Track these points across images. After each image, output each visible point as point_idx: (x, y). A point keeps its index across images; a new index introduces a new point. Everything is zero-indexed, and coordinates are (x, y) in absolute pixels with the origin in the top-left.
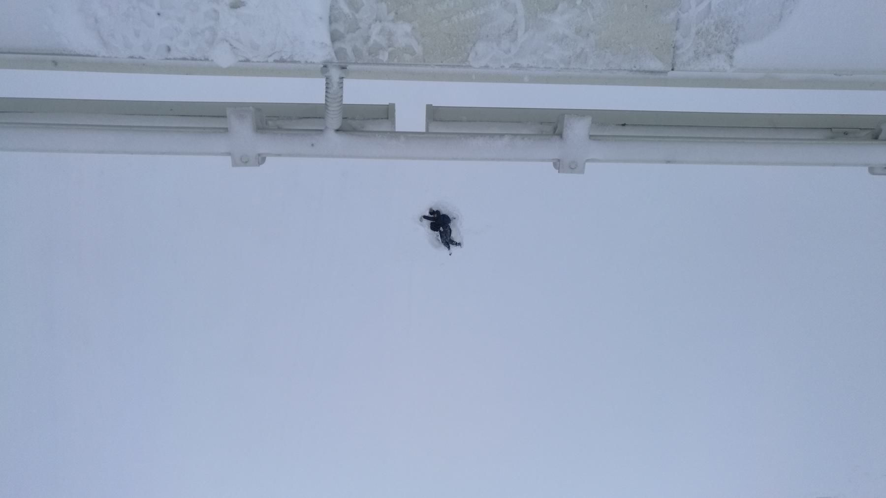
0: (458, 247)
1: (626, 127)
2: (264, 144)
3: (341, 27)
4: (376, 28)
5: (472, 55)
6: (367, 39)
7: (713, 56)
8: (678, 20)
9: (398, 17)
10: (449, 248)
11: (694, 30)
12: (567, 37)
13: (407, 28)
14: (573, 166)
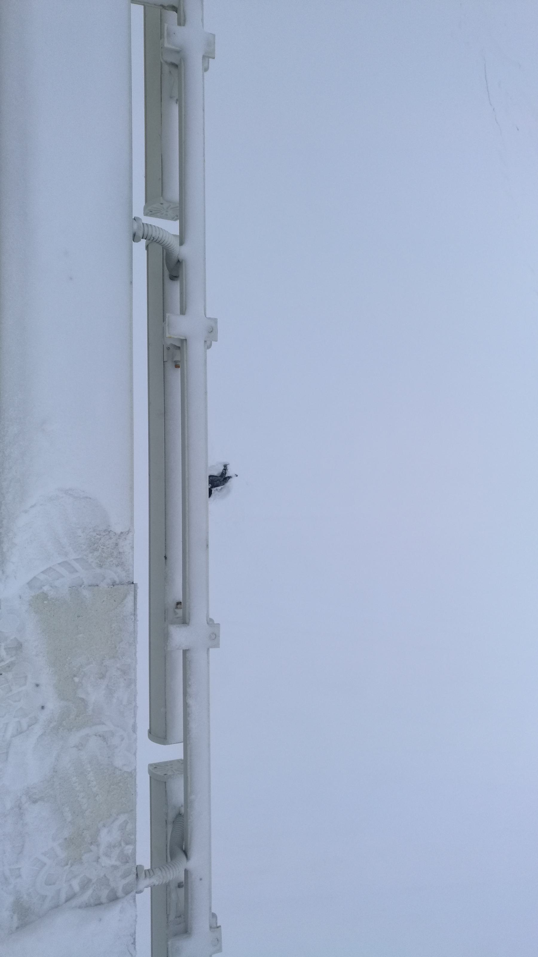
0: (228, 467)
1: (168, 557)
2: (201, 924)
3: (104, 894)
4: (106, 862)
5: (125, 769)
6: (115, 867)
7: (121, 550)
8: (90, 586)
9: (94, 841)
10: (229, 477)
11: (98, 570)
12: (107, 686)
13: (104, 832)
14: (213, 637)
